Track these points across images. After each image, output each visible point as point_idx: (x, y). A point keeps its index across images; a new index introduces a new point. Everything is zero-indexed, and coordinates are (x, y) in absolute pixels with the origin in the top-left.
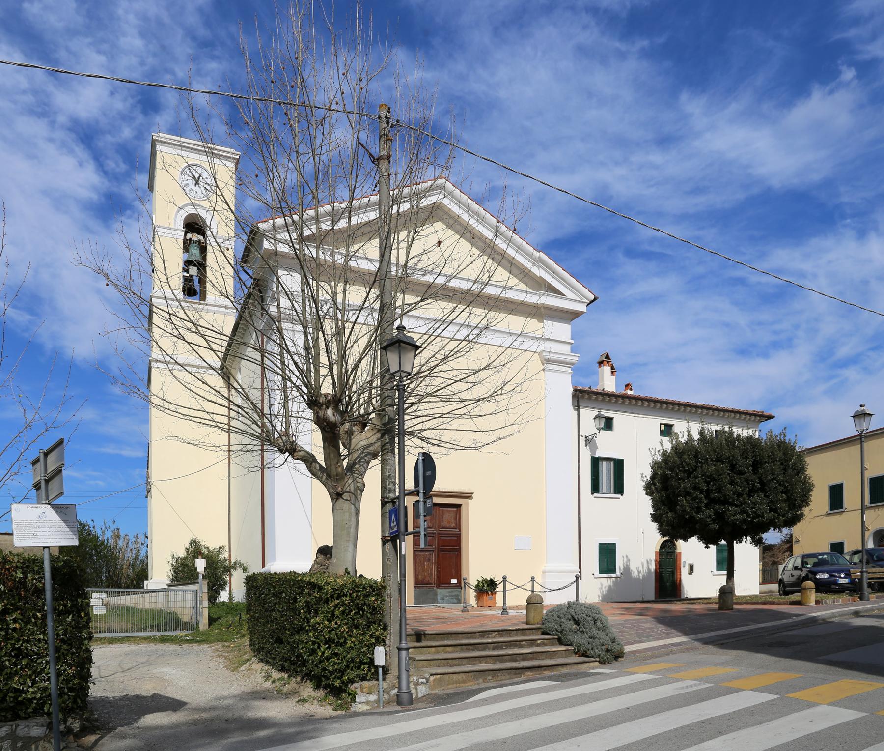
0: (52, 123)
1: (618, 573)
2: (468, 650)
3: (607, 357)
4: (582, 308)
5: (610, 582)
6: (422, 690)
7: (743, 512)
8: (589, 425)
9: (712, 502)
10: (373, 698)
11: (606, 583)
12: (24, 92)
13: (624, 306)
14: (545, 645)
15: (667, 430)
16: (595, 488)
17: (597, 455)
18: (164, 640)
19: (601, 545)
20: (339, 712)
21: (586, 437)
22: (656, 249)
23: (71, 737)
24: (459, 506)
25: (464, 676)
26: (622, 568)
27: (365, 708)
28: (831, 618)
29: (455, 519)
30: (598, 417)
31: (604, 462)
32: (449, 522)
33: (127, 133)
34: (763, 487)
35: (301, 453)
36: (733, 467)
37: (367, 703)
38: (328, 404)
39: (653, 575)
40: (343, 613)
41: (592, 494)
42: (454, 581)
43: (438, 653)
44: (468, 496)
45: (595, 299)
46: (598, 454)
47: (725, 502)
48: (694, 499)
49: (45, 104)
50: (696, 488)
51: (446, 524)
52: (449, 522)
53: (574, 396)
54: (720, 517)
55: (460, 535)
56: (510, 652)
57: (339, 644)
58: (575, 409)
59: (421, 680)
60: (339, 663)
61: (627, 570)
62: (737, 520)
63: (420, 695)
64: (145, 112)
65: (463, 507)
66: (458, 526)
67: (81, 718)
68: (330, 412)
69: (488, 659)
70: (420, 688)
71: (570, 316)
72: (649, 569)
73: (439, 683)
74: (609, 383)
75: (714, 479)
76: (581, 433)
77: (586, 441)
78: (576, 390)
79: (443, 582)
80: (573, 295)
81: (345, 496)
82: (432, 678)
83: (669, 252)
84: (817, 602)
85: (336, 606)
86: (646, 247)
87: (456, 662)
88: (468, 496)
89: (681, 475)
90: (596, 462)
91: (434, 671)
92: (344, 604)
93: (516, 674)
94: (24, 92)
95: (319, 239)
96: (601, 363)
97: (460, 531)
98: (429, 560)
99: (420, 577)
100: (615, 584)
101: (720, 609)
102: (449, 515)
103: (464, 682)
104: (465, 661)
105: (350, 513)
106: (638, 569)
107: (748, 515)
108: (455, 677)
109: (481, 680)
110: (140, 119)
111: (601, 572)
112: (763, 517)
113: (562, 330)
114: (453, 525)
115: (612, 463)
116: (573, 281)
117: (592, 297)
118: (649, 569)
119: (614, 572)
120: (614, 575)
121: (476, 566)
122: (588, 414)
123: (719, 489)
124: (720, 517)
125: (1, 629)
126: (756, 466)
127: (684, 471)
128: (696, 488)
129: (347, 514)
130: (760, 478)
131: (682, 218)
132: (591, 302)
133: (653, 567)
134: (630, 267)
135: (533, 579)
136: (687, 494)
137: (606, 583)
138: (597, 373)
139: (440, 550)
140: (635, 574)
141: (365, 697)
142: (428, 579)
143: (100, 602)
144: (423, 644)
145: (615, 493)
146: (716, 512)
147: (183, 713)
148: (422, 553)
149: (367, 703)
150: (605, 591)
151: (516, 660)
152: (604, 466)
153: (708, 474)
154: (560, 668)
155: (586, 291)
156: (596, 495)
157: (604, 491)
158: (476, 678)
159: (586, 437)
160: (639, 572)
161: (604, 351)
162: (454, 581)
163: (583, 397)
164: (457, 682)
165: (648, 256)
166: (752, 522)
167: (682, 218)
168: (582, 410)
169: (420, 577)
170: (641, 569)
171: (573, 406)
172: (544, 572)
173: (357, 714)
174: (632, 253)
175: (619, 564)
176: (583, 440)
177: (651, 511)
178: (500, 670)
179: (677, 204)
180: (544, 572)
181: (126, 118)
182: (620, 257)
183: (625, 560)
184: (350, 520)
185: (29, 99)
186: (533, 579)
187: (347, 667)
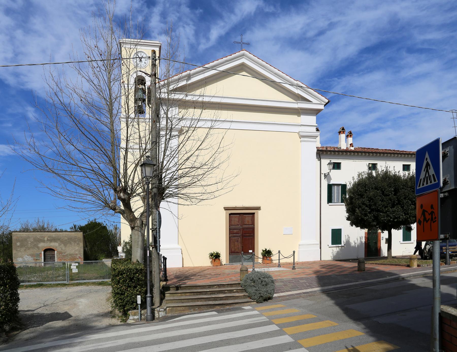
0: (105, 19)
1: (343, 244)
2: (197, 295)
3: (343, 129)
4: (322, 107)
5: (338, 249)
6: (162, 314)
7: (388, 216)
8: (326, 169)
9: (372, 210)
10: (136, 317)
11: (336, 249)
12: (92, 5)
13: (406, 82)
14: (238, 292)
15: (374, 167)
16: (330, 200)
17: (331, 183)
18: (100, 284)
19: (333, 230)
20: (122, 323)
21: (325, 174)
22: (426, 46)
23: (4, 333)
24: (254, 213)
25: (184, 308)
26: (345, 241)
27: (133, 321)
28: (407, 277)
29: (252, 220)
30: (329, 164)
31: (336, 187)
32: (248, 222)
33: (140, 18)
34: (399, 203)
35: (118, 210)
36: (383, 193)
37: (134, 319)
38: (121, 191)
39: (364, 245)
40: (124, 281)
41: (328, 203)
42: (251, 251)
43: (182, 296)
44: (258, 208)
45: (328, 102)
46: (331, 183)
47: (378, 211)
48: (363, 210)
49: (101, 10)
50: (363, 204)
51: (246, 223)
52: (248, 222)
53: (317, 153)
54: (376, 218)
55: (254, 228)
56: (213, 296)
57: (122, 294)
58: (318, 160)
59: (161, 310)
60: (122, 303)
61: (348, 242)
62: (385, 220)
63: (160, 316)
64: (148, 7)
65: (255, 214)
66: (253, 224)
67: (9, 325)
68: (122, 194)
69: (202, 300)
70: (160, 313)
71: (316, 112)
72: (361, 242)
73: (171, 311)
74: (344, 143)
75: (372, 199)
76: (322, 172)
77: (325, 176)
78: (318, 150)
79: (246, 252)
80: (317, 101)
81: (136, 228)
82: (168, 309)
83: (434, 47)
84: (418, 266)
85: (120, 278)
86: (420, 46)
87: (186, 300)
88: (258, 208)
89: (357, 197)
90: (330, 187)
91: (168, 306)
92: (123, 278)
93: (210, 307)
94: (92, 5)
95: (175, 90)
96: (340, 133)
97: (254, 226)
98: (238, 241)
99: (233, 250)
100: (341, 250)
101: (358, 270)
102: (248, 218)
103: (184, 310)
104: (190, 300)
105: (139, 236)
106: (354, 242)
107: (391, 218)
108: (179, 308)
109: (192, 310)
110: (146, 10)
111: (332, 244)
112: (399, 217)
113: (312, 120)
114: (250, 223)
115: (340, 187)
116: (316, 94)
117: (327, 101)
118: (361, 242)
119: (341, 244)
120: (340, 245)
121: (262, 242)
122: (325, 162)
123: (375, 204)
124: (376, 218)
125: (0, 286)
126: (396, 191)
127: (359, 195)
128: (363, 204)
129: (137, 236)
130: (397, 198)
131: (442, 27)
132: (327, 104)
133: (363, 240)
134: (410, 59)
135: (279, 252)
136: (360, 207)
137: (336, 249)
138: (338, 137)
139: (243, 236)
140: (353, 244)
141: (133, 317)
142: (237, 250)
143: (75, 267)
144: (179, 291)
145: (341, 202)
146: (374, 216)
147: (68, 322)
148: (234, 238)
149: (134, 319)
150: (335, 254)
151: (217, 300)
152: (335, 189)
153: (369, 196)
154: (234, 305)
155: (323, 98)
156: (330, 204)
157: (335, 202)
158: (190, 309)
159: (325, 174)
160: (355, 243)
161: (341, 127)
162: (251, 251)
163: (323, 153)
164: (180, 311)
165: (421, 51)
166: (393, 221)
167: (442, 27)
168: (322, 160)
169: (233, 250)
170: (356, 241)
171: (317, 158)
172: (299, 245)
173: (130, 325)
174: (411, 50)
175: (343, 239)
176: (323, 176)
177: (347, 215)
178: (202, 305)
179: (439, 19)
180: (299, 245)
181: (139, 11)
182: (404, 54)
183: (347, 237)
184: (138, 239)
185: (94, 8)
186: (279, 252)
187: (126, 304)
